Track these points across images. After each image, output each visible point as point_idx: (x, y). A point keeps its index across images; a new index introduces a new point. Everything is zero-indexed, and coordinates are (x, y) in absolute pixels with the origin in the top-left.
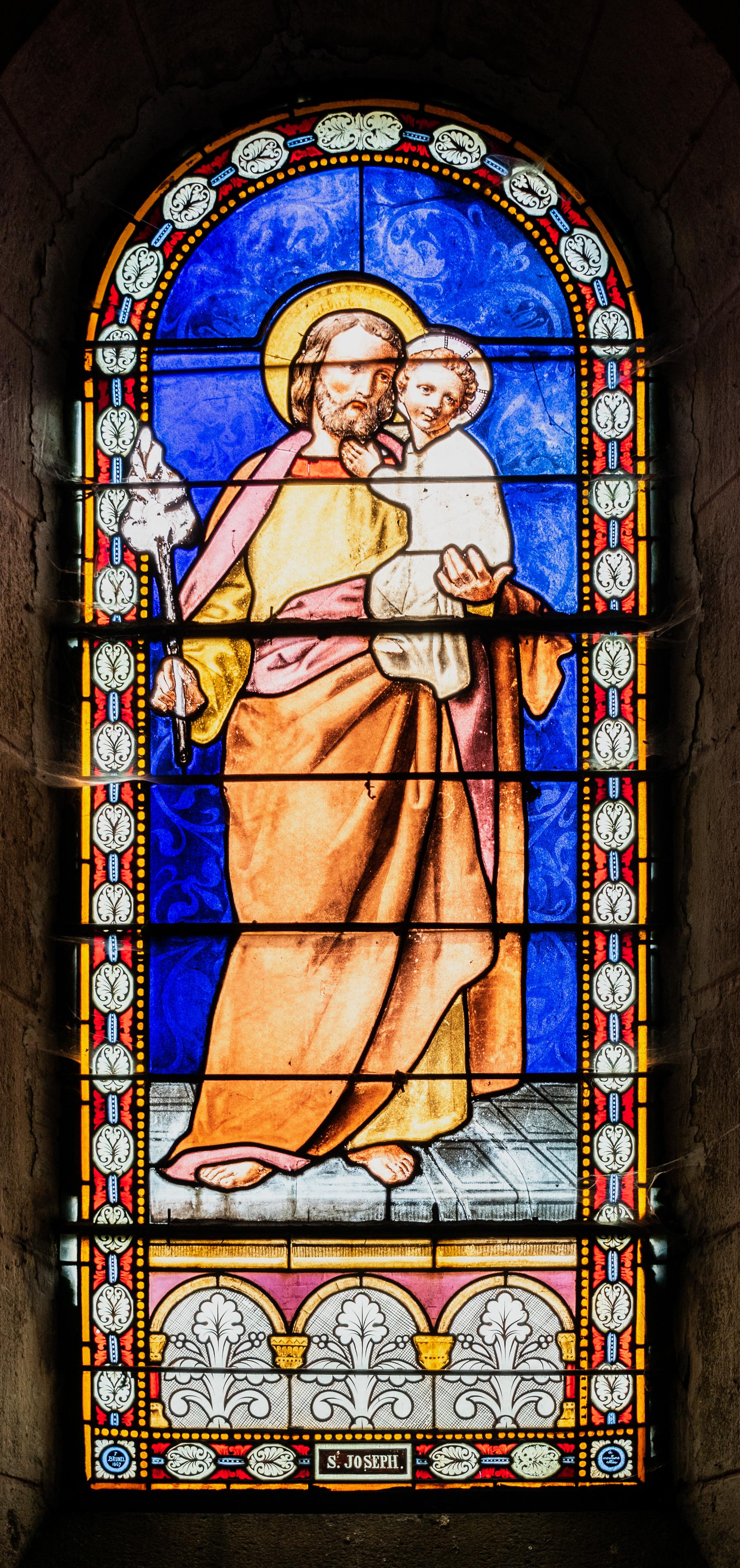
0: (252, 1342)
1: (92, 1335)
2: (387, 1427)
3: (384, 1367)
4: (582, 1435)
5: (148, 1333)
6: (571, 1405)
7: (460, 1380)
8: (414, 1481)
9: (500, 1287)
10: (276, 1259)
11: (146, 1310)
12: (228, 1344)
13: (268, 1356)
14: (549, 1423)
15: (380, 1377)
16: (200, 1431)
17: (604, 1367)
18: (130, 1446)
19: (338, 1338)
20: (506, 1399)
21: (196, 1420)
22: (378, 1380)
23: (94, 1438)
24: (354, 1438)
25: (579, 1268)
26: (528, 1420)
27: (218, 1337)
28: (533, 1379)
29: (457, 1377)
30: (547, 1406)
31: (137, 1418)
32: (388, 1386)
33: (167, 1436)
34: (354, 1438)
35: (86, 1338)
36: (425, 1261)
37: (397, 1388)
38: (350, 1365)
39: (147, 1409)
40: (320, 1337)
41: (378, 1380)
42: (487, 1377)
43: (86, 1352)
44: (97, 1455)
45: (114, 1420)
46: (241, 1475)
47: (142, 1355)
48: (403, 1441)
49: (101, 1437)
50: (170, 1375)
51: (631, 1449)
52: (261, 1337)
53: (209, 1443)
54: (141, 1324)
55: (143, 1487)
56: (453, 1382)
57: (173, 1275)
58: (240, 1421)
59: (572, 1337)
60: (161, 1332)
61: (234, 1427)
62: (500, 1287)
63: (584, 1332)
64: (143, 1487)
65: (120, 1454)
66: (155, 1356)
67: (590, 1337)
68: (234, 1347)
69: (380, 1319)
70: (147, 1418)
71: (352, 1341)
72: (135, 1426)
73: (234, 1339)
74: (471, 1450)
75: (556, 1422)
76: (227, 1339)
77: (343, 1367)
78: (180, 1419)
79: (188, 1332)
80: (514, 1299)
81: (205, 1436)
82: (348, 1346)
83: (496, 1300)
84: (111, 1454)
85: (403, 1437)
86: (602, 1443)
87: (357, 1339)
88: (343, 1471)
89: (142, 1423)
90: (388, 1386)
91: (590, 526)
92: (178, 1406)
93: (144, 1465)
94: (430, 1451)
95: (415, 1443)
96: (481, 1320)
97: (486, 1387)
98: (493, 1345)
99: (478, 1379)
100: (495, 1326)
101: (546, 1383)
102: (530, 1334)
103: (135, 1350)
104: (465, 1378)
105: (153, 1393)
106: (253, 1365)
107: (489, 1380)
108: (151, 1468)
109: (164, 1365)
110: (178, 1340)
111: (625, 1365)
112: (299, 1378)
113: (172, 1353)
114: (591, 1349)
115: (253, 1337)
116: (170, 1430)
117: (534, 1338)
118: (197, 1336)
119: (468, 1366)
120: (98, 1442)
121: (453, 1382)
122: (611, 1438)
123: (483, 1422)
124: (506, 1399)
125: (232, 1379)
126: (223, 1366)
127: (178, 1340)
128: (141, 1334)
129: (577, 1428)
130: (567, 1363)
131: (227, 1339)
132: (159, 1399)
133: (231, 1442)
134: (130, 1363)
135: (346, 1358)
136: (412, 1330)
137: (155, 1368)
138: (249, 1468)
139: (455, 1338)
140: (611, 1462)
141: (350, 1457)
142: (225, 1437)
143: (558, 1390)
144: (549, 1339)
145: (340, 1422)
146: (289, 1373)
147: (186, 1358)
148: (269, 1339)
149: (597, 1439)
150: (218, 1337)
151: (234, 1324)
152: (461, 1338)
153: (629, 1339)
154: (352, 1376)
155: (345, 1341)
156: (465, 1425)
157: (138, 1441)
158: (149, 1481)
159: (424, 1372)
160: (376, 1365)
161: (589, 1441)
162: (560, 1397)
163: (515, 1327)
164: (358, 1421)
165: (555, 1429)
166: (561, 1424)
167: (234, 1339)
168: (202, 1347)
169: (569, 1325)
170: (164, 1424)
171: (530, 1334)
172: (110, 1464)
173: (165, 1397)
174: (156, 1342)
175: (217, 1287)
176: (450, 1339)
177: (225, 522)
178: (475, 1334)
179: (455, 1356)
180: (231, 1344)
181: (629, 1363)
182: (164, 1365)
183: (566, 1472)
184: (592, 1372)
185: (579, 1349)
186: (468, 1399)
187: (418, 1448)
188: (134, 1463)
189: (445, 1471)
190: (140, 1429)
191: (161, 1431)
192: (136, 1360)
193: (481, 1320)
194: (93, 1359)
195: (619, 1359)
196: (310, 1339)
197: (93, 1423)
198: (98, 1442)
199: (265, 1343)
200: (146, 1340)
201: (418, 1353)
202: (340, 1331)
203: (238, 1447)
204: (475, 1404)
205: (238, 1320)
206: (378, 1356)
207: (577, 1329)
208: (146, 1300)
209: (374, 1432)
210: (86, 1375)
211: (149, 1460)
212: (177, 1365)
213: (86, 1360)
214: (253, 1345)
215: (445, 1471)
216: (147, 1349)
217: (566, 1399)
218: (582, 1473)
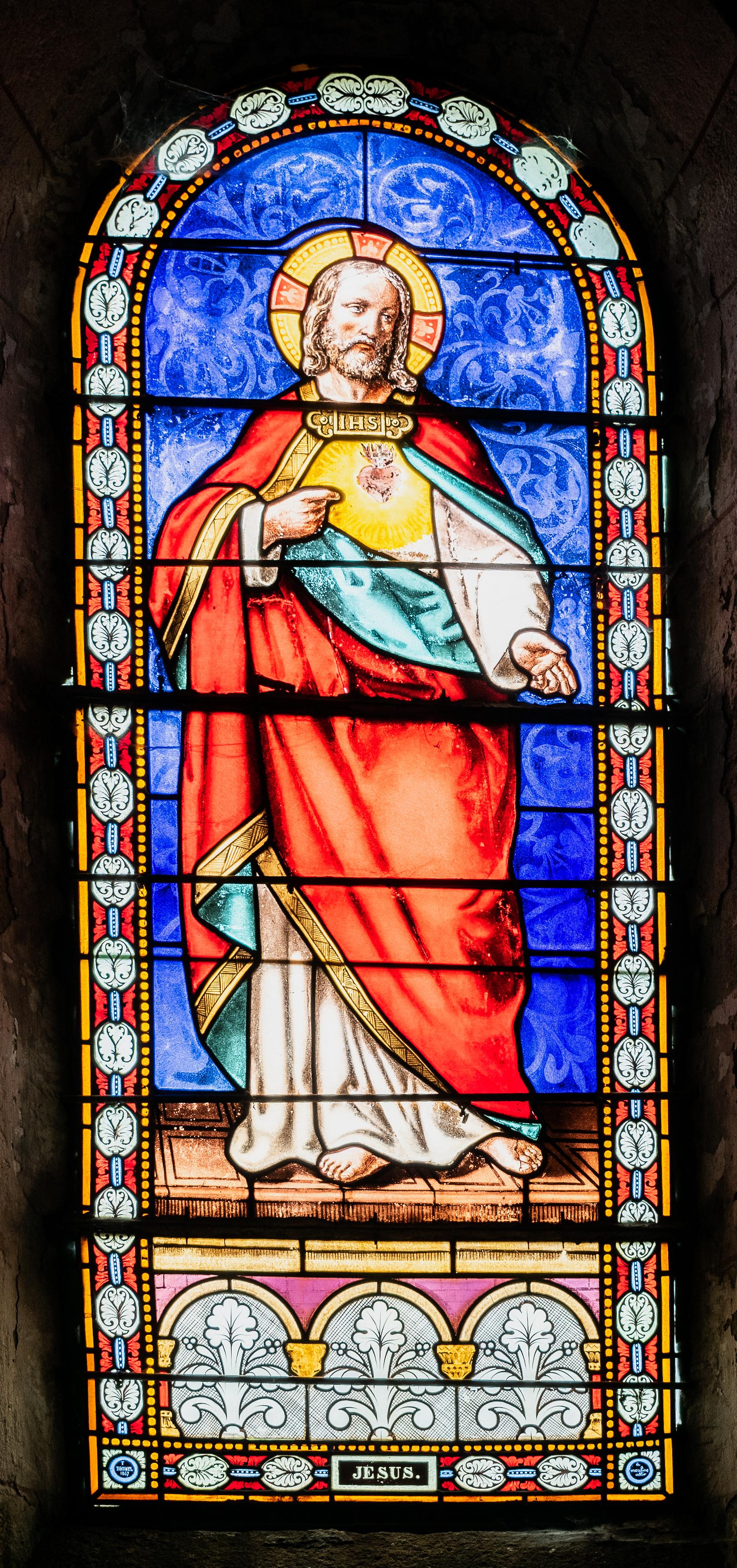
0: (267, 1348)
1: (96, 1341)
2: (475, 1438)
3: (407, 1376)
4: (610, 1446)
5: (156, 1337)
6: (598, 1416)
7: (333, 1389)
8: (441, 1492)
9: (372, 1295)
10: (289, 1262)
11: (153, 1312)
12: (538, 1353)
13: (433, 1366)
14: (575, 1434)
15: (400, 1387)
16: (214, 1441)
17: (630, 1379)
18: (140, 1456)
19: (506, 1346)
20: (382, 1410)
21: (207, 1430)
22: (250, 1387)
23: (101, 1447)
24: (347, 1449)
25: (601, 1276)
26: (553, 1431)
27: (529, 1345)
28: (409, 1390)
29: (329, 1387)
30: (573, 1416)
31: (146, 1427)
32: (409, 1396)
33: (178, 1445)
34: (347, 1449)
35: (90, 1344)
36: (442, 1265)
37: (417, 1398)
38: (369, 1373)
39: (157, 1417)
40: (487, 1344)
41: (399, 1389)
42: (362, 1387)
43: (90, 1358)
44: (105, 1465)
45: (123, 1429)
46: (256, 1486)
47: (150, 1361)
48: (430, 1453)
49: (110, 1447)
50: (179, 1383)
51: (659, 1459)
52: (573, 1345)
53: (222, 1454)
54: (148, 1329)
55: (155, 1497)
56: (326, 1391)
57: (492, 1280)
58: (258, 1431)
59: (597, 1347)
60: (170, 1337)
61: (548, 1438)
62: (372, 1295)
63: (609, 1343)
64: (155, 1497)
65: (127, 1464)
66: (164, 1363)
67: (614, 1347)
68: (248, 1353)
69: (398, 1327)
70: (158, 1427)
71: (519, 1349)
72: (145, 1436)
73: (248, 1345)
74: (579, 1461)
75: (582, 1434)
76: (538, 1349)
77: (213, 1373)
78: (280, 1431)
79: (497, 1341)
80: (239, 1304)
81: (219, 1447)
82: (367, 1353)
83: (222, 1304)
84: (119, 1464)
85: (400, 1449)
86: (629, 1455)
87: (524, 1346)
88: (375, 1482)
89: (152, 1432)
90: (409, 1396)
91: (133, 524)
92: (189, 1413)
93: (155, 1475)
94: (263, 1463)
95: (440, 1455)
96: (355, 1327)
97: (512, 1398)
98: (516, 1353)
99: (352, 1388)
100: (370, 1334)
101: (349, 1393)
102: (554, 1342)
103: (143, 1355)
104: (191, 1384)
105: (164, 1402)
106: (421, 1376)
107: (364, 1390)
108: (162, 1479)
109: (174, 1372)
110: (487, 1348)
111: (652, 1377)
112: (315, 1387)
113: (184, 1357)
114: (616, 1358)
115: (268, 1343)
116: (183, 1439)
117: (558, 1345)
118: (209, 1340)
119: (338, 1375)
120: (105, 1452)
121: (326, 1391)
122: (639, 1450)
123: (506, 1432)
124: (382, 1410)
125: (395, 1389)
126: (236, 1373)
127: (487, 1348)
128: (149, 1338)
129: (604, 1440)
130: (591, 1373)
131: (538, 1349)
132: (169, 1408)
133: (245, 1452)
134: (138, 1370)
135: (365, 1365)
136: (580, 1338)
137: (165, 1377)
138: (180, 1478)
139: (477, 1347)
140: (640, 1474)
141: (359, 1468)
142: (239, 1447)
143: (583, 1400)
144: (277, 1344)
145: (359, 1432)
146: (307, 1381)
147: (351, 1368)
148: (284, 1345)
149: (625, 1450)
150: (231, 1342)
151: (248, 1330)
152: (483, 1346)
153: (655, 1350)
154: (371, 1387)
155: (513, 1348)
156: (489, 1436)
157: (148, 1451)
158: (161, 1491)
159: (447, 1382)
160: (399, 1372)
161: (616, 1452)
162: (586, 1410)
163: (389, 1337)
164: (378, 1432)
165: (582, 1440)
166: (589, 1435)
167: (248, 1345)
168: (513, 1357)
169: (593, 1334)
170: (175, 1433)
171: (554, 1342)
172: (118, 1473)
173: (175, 1407)
174: (165, 1347)
175: (230, 1290)
176: (472, 1348)
177: (429, 503)
178: (497, 1341)
179: (328, 1365)
180: (542, 1353)
181: (655, 1375)
182: (174, 1372)
183: (597, 1485)
184: (617, 1384)
185: (604, 1359)
186: (196, 1406)
187: (166, 1457)
188: (144, 1473)
189: (553, 1482)
190: (151, 1439)
191: (172, 1440)
192: (144, 1366)
193: (355, 1327)
194: (98, 1365)
195: (645, 1371)
196: (477, 1347)
197: (100, 1433)
198: (105, 1452)
199: (280, 1350)
200: (154, 1344)
201: (290, 1361)
202: (506, 1339)
203: (529, 1458)
204: (350, 1414)
205: (253, 1325)
206: (397, 1365)
207: (602, 1340)
208: (153, 1303)
209: (395, 1442)
210: (91, 1383)
211: (159, 1471)
212: (189, 1372)
213: (91, 1367)
214: (565, 1354)
215: (553, 1482)
216: (155, 1355)
217: (592, 1411)
218: (610, 1485)
